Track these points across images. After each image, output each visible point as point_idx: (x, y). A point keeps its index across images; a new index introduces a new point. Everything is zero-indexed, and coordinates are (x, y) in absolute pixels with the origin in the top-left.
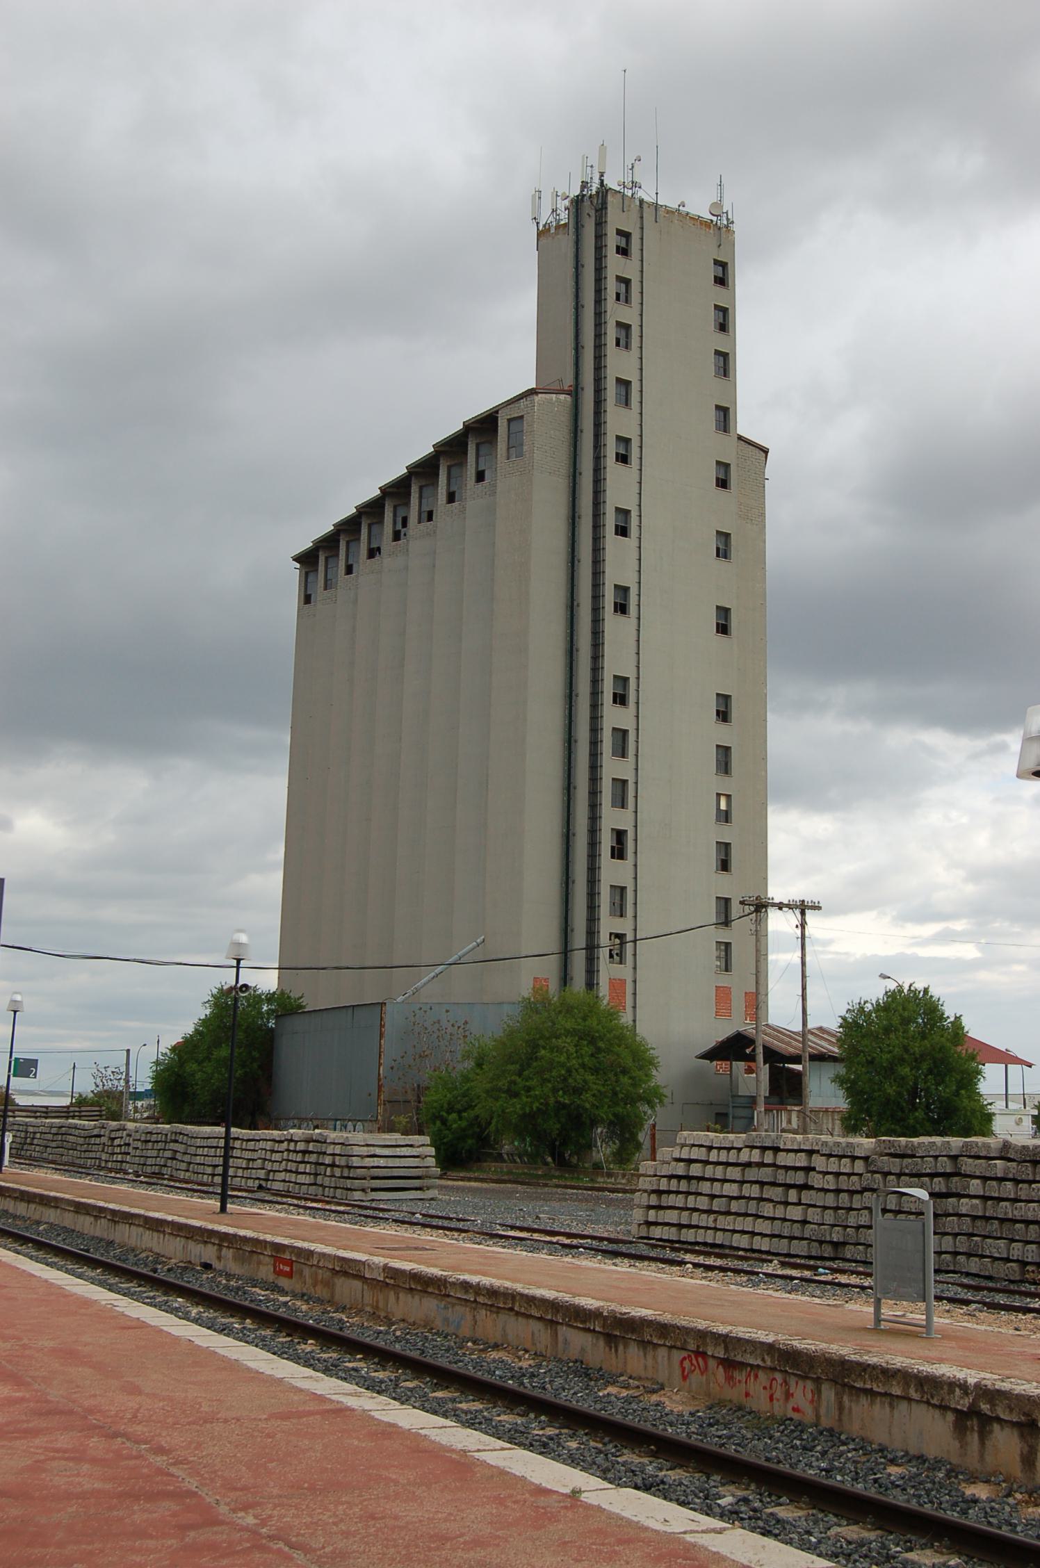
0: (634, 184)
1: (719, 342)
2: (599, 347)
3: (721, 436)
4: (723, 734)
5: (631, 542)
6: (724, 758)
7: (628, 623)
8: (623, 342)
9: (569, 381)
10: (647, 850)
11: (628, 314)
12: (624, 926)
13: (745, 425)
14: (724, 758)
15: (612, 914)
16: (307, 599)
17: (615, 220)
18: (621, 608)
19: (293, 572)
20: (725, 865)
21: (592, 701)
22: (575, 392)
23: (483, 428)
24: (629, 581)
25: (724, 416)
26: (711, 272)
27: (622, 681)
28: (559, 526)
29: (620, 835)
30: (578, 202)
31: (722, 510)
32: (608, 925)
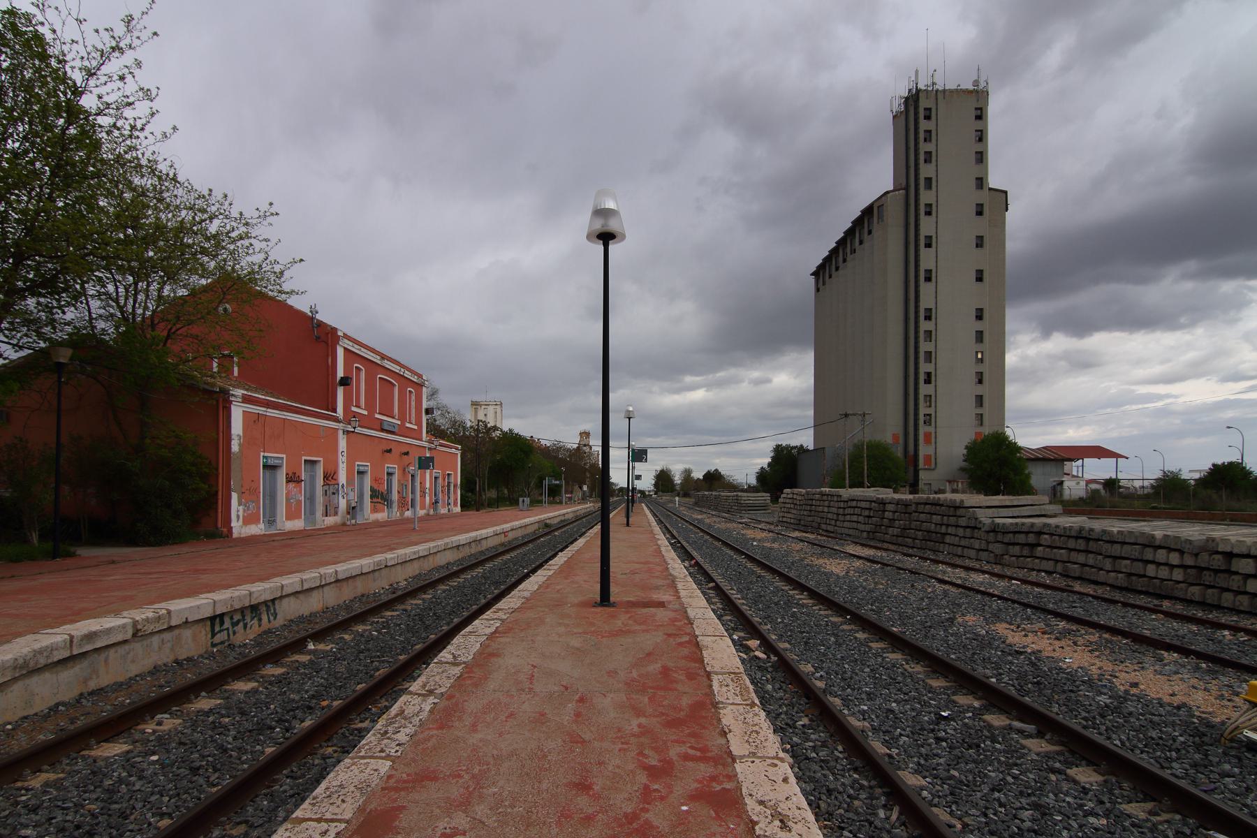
0: (934, 84)
1: (979, 148)
2: (917, 165)
3: (980, 192)
4: (979, 390)
5: (933, 250)
6: (980, 400)
7: (931, 285)
8: (928, 159)
9: (904, 184)
10: (941, 381)
11: (930, 147)
12: (931, 411)
13: (994, 181)
14: (980, 336)
15: (926, 361)
16: (818, 290)
17: (923, 103)
18: (928, 279)
19: (812, 279)
20: (980, 382)
21: (916, 319)
22: (907, 188)
23: (868, 211)
24: (932, 266)
25: (981, 182)
26: (973, 113)
27: (929, 272)
28: (900, 328)
29: (929, 374)
30: (907, 99)
31: (980, 226)
32: (923, 410)
